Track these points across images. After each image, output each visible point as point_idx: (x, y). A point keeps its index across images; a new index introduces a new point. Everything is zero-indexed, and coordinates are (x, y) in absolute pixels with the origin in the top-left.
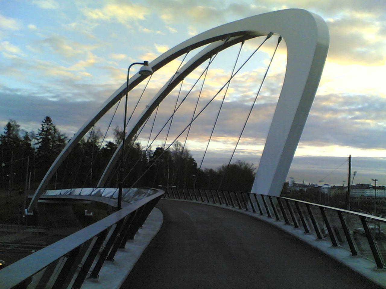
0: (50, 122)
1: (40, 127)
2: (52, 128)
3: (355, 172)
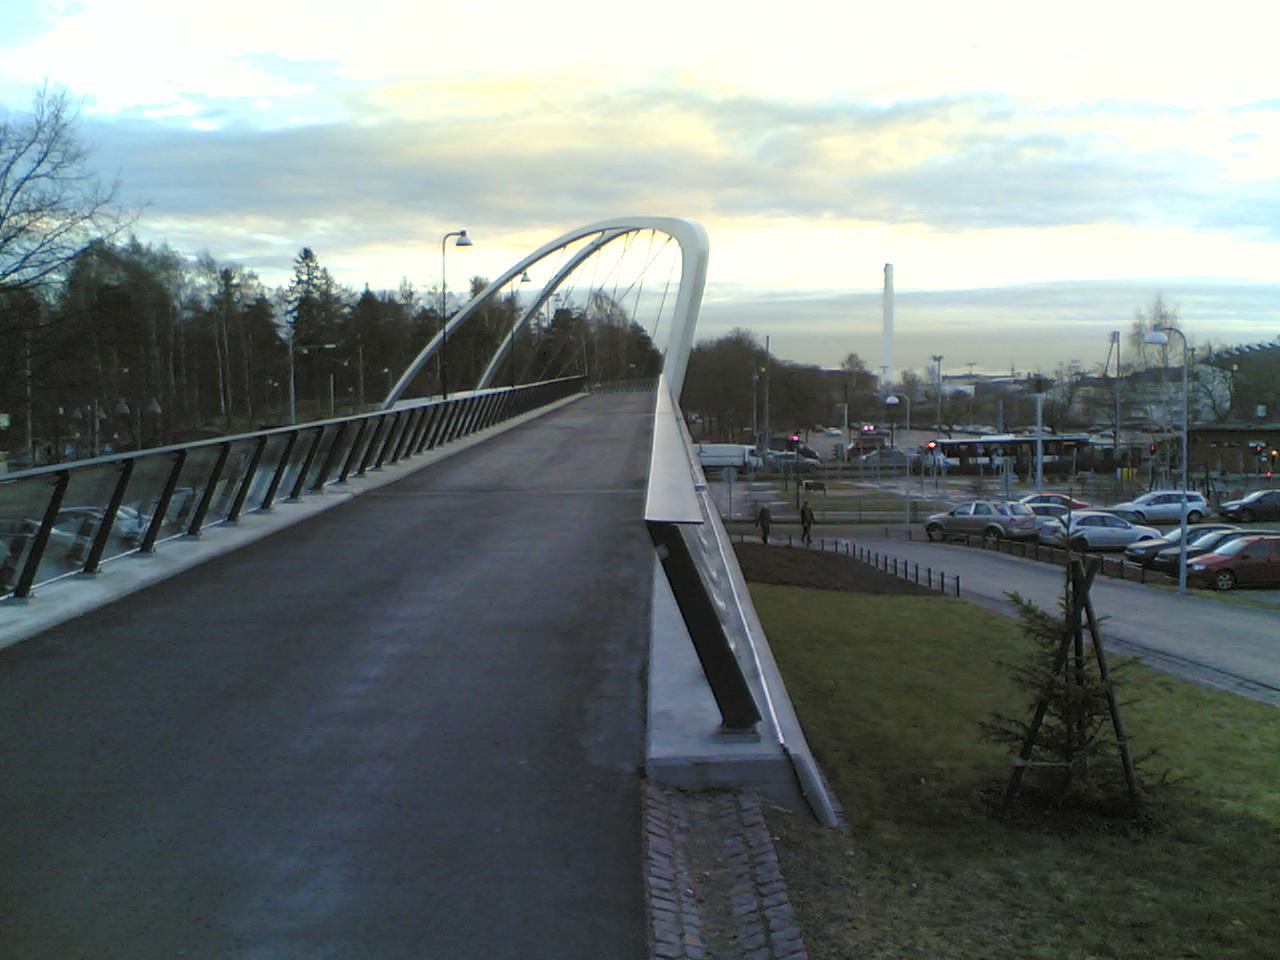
0: (312, 261)
1: (293, 275)
2: (318, 274)
3: (1115, 333)
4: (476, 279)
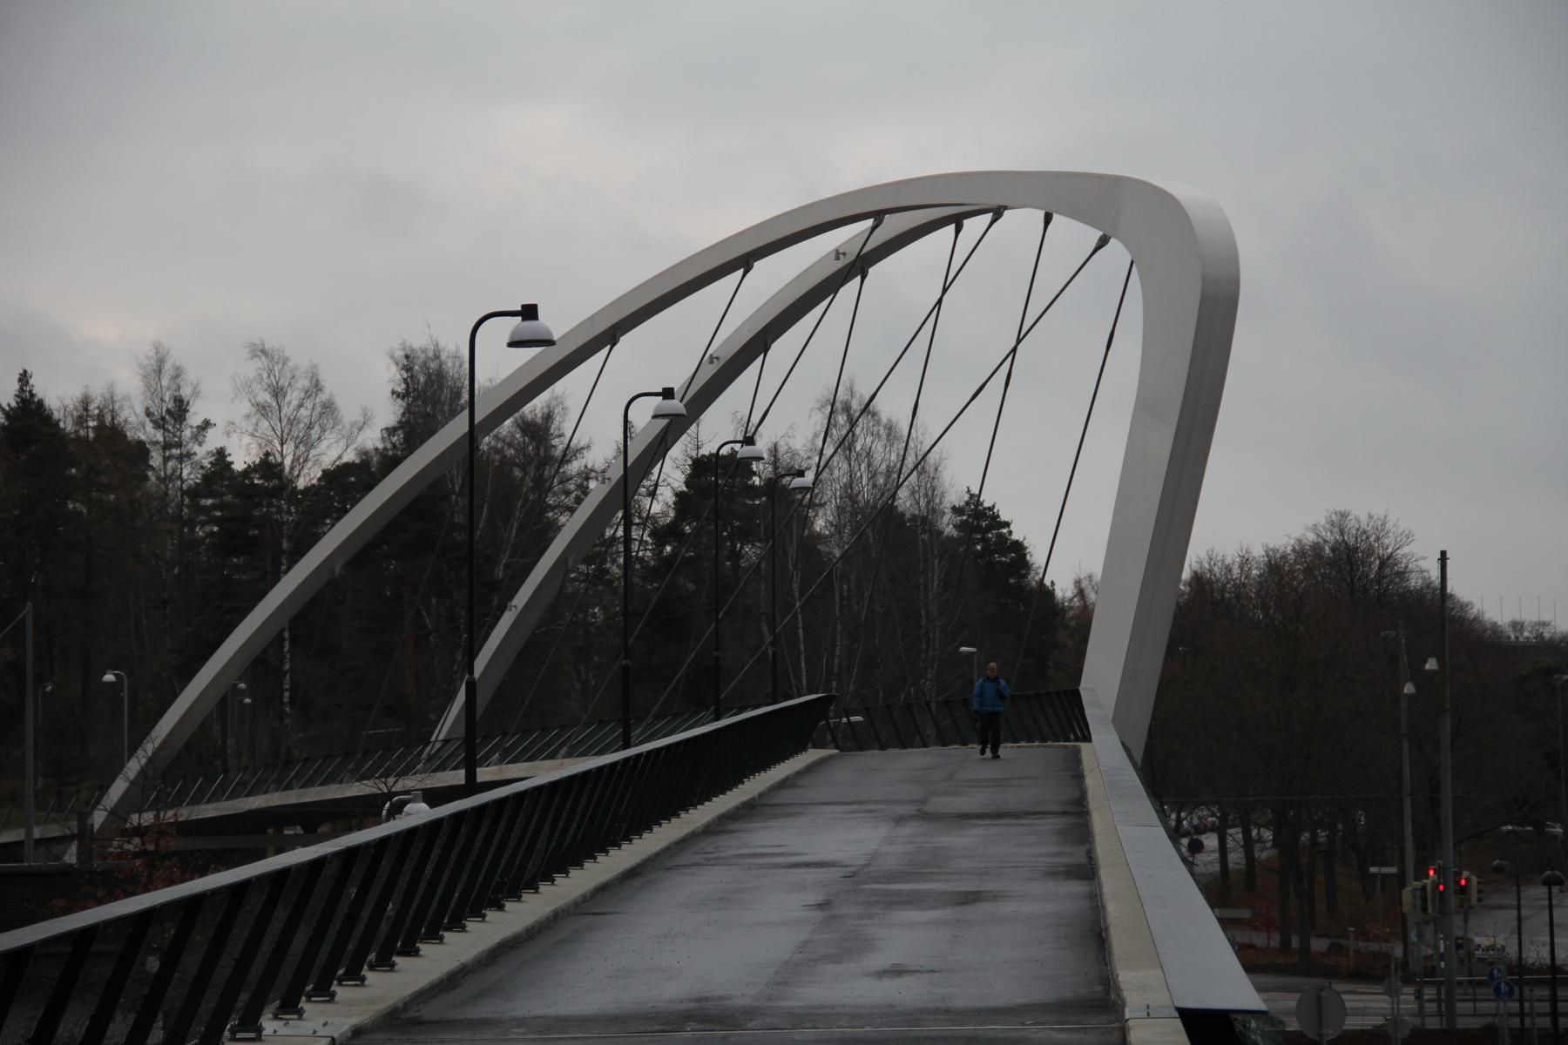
4: (403, 343)
